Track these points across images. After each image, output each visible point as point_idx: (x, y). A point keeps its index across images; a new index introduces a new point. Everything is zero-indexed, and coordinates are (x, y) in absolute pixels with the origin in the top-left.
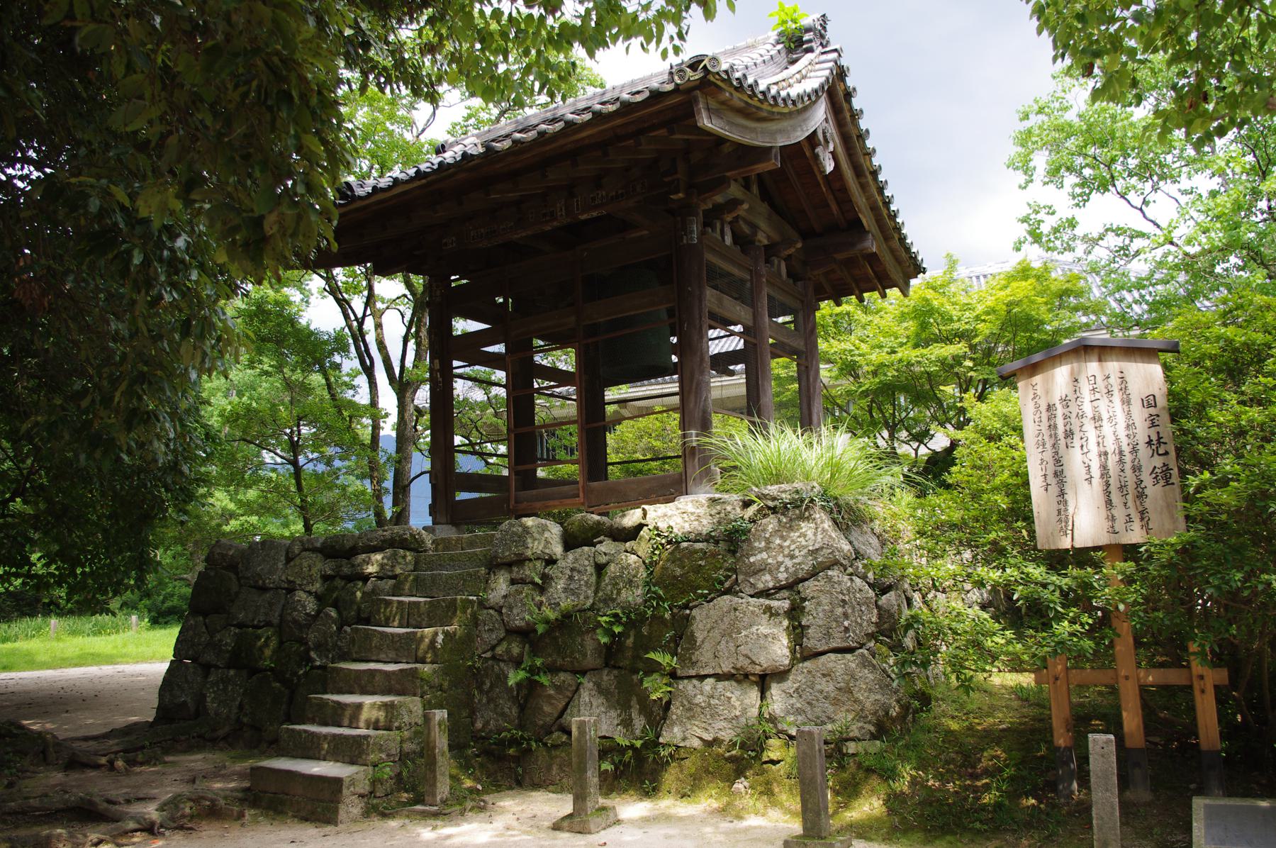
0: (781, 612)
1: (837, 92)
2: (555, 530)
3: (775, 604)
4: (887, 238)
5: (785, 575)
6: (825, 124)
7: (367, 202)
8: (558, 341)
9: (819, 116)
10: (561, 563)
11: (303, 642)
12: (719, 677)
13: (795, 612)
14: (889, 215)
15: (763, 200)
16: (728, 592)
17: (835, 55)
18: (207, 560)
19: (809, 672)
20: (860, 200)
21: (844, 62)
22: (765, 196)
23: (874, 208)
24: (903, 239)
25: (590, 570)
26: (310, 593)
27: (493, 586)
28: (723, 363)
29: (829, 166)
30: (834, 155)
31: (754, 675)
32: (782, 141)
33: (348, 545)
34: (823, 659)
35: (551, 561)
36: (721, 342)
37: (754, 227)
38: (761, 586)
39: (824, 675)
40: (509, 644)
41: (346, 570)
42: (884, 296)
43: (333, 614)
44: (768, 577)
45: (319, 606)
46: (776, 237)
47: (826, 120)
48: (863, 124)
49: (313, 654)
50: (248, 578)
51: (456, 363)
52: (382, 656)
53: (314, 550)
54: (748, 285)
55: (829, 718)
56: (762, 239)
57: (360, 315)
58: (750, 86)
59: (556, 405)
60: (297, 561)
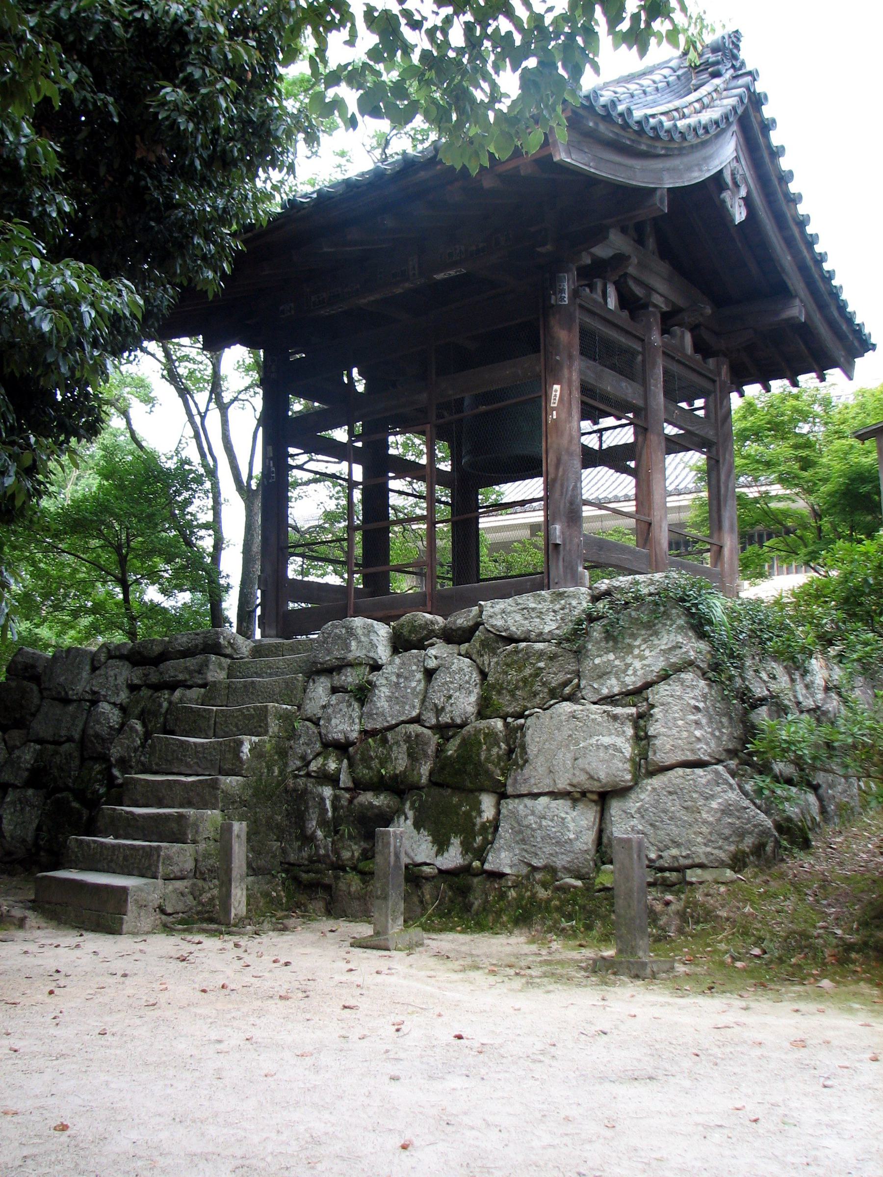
1: (750, 124)
2: (383, 631)
3: (618, 710)
4: (822, 307)
5: (633, 678)
6: (735, 164)
9: (726, 153)
10: (387, 670)
11: (104, 758)
12: (554, 795)
13: (641, 720)
14: (823, 277)
16: (569, 698)
17: (748, 79)
18: (8, 671)
19: (654, 789)
20: (786, 260)
21: (759, 87)
22: (665, 252)
23: (803, 269)
24: (842, 307)
25: (419, 676)
26: (114, 704)
29: (739, 214)
30: (748, 201)
31: (592, 792)
32: (669, 183)
33: (157, 649)
34: (670, 773)
35: (376, 667)
37: (650, 289)
38: (605, 691)
39: (670, 793)
40: (326, 758)
41: (154, 679)
42: (822, 379)
43: (139, 727)
44: (614, 681)
45: (123, 718)
46: (680, 302)
47: (737, 159)
48: (785, 163)
50: (50, 689)
51: (292, 450)
53: (121, 657)
55: (674, 842)
57: (202, 410)
58: (621, 115)
60: (102, 671)
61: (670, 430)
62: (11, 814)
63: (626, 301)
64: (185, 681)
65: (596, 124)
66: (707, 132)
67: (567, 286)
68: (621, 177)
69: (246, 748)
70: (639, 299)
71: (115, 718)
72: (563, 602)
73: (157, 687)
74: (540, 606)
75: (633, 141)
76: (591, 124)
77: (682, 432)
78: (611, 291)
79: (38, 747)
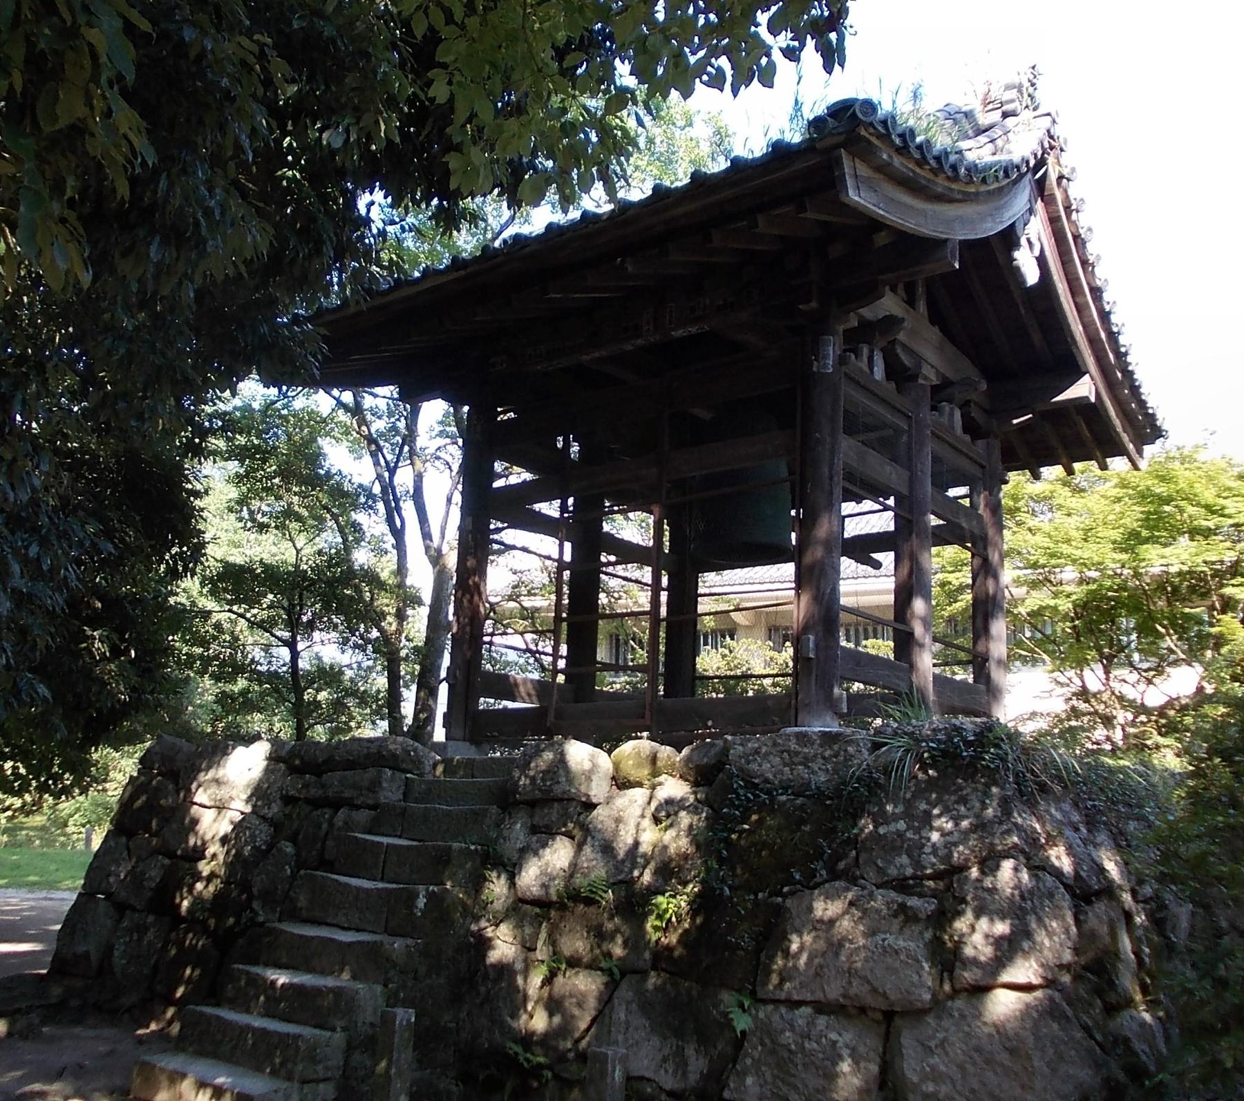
0: (923, 916)
3: (913, 902)
7: (391, 297)
8: (631, 501)
12: (821, 1008)
15: (933, 324)
21: (1056, 131)
27: (505, 833)
28: (863, 549)
29: (1032, 276)
30: (1042, 261)
36: (867, 518)
37: (919, 359)
38: (893, 872)
41: (314, 792)
44: (904, 859)
46: (950, 375)
49: (256, 905)
52: (342, 920)
54: (905, 438)
56: (930, 375)
58: (920, 147)
59: (629, 590)
61: (934, 521)
62: (126, 944)
63: (895, 371)
64: (352, 798)
65: (890, 157)
66: (1007, 175)
67: (832, 350)
68: (911, 224)
69: (421, 902)
70: (906, 369)
71: (263, 835)
72: (836, 747)
73: (316, 803)
74: (806, 750)
75: (929, 180)
76: (885, 156)
77: (942, 522)
78: (879, 359)
79: (167, 861)
